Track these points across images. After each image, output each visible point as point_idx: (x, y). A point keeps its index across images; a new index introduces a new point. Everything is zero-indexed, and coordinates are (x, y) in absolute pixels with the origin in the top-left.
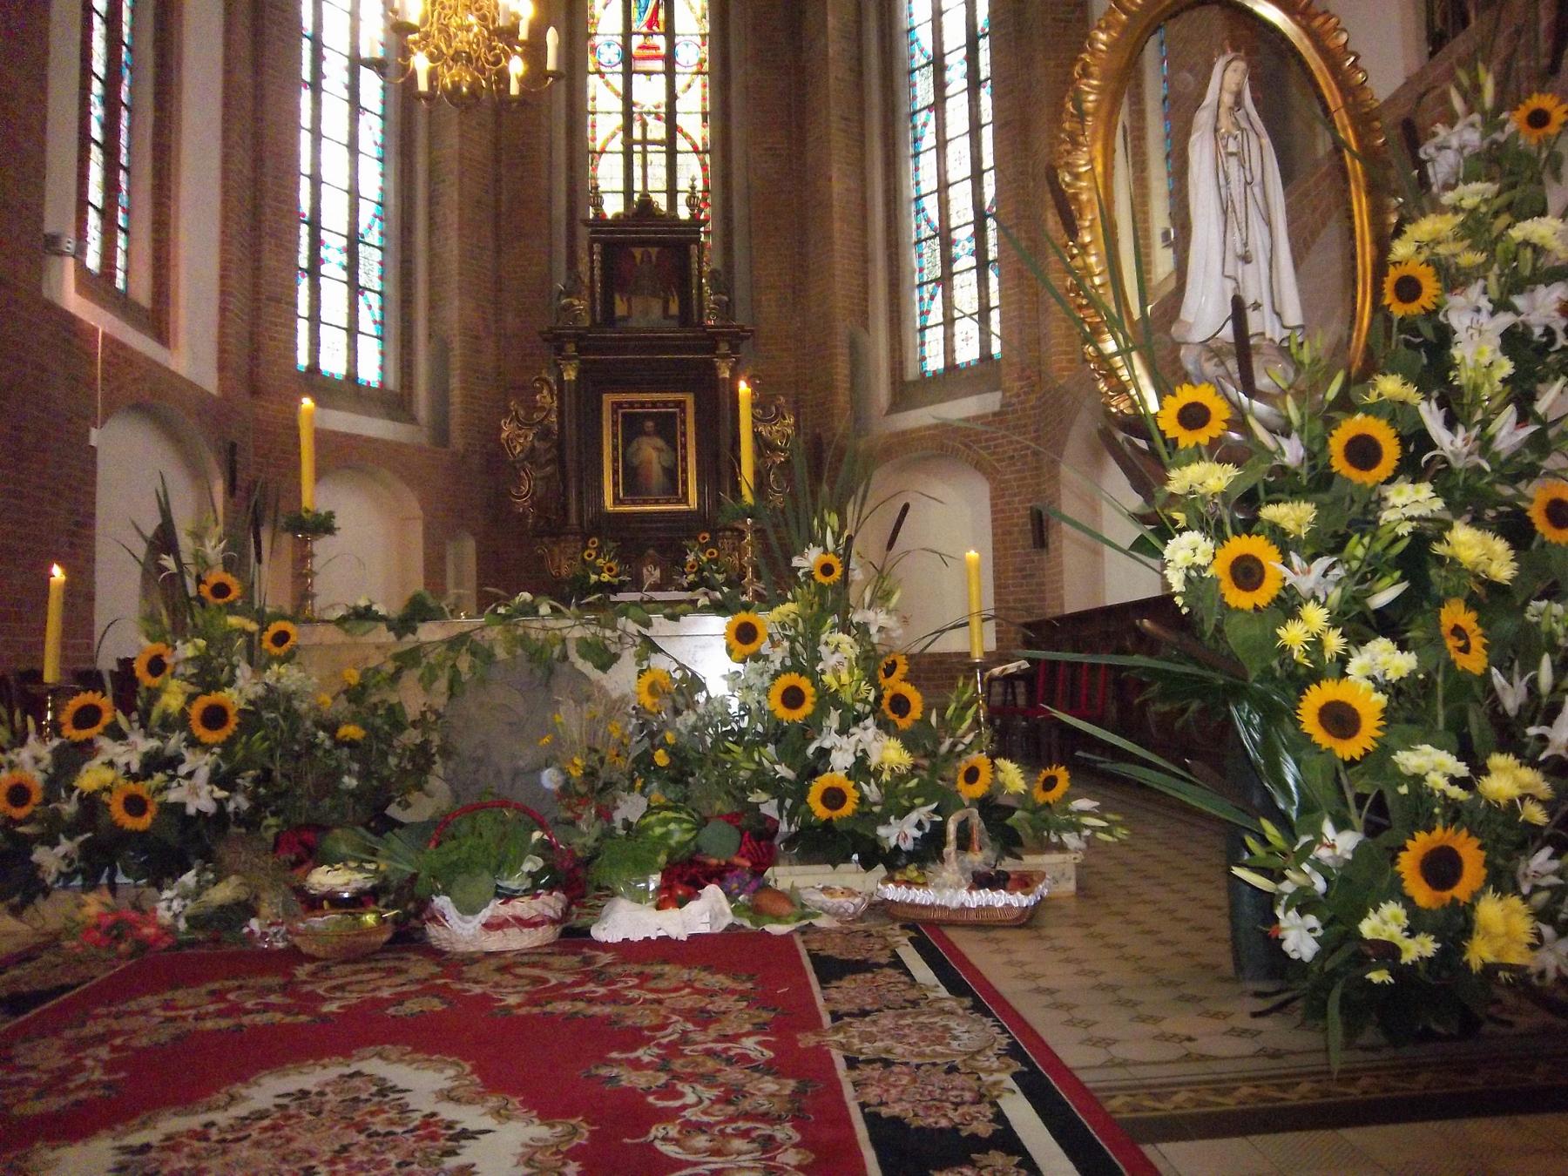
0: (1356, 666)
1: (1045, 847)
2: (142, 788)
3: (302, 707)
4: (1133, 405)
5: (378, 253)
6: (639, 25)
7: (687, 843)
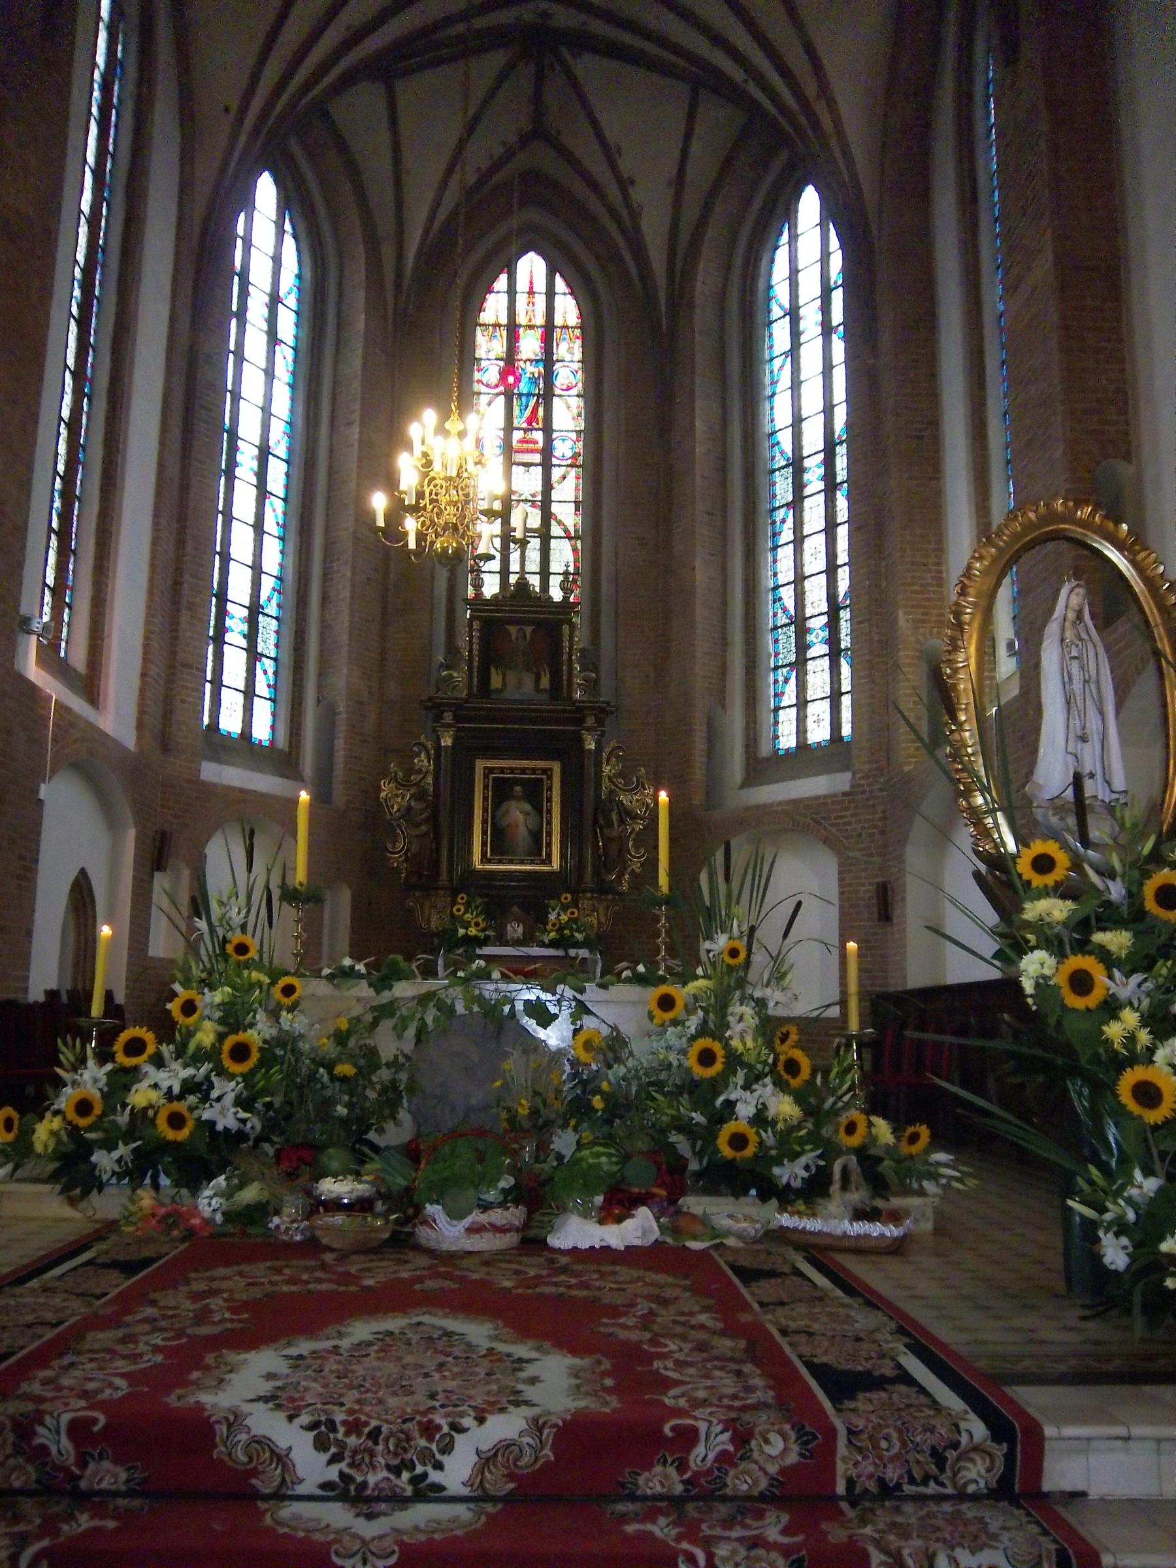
0: (1161, 1055)
1: (907, 1192)
2: (181, 1107)
3: (304, 1046)
4: (996, 847)
5: (275, 622)
6: (519, 421)
7: (615, 1174)
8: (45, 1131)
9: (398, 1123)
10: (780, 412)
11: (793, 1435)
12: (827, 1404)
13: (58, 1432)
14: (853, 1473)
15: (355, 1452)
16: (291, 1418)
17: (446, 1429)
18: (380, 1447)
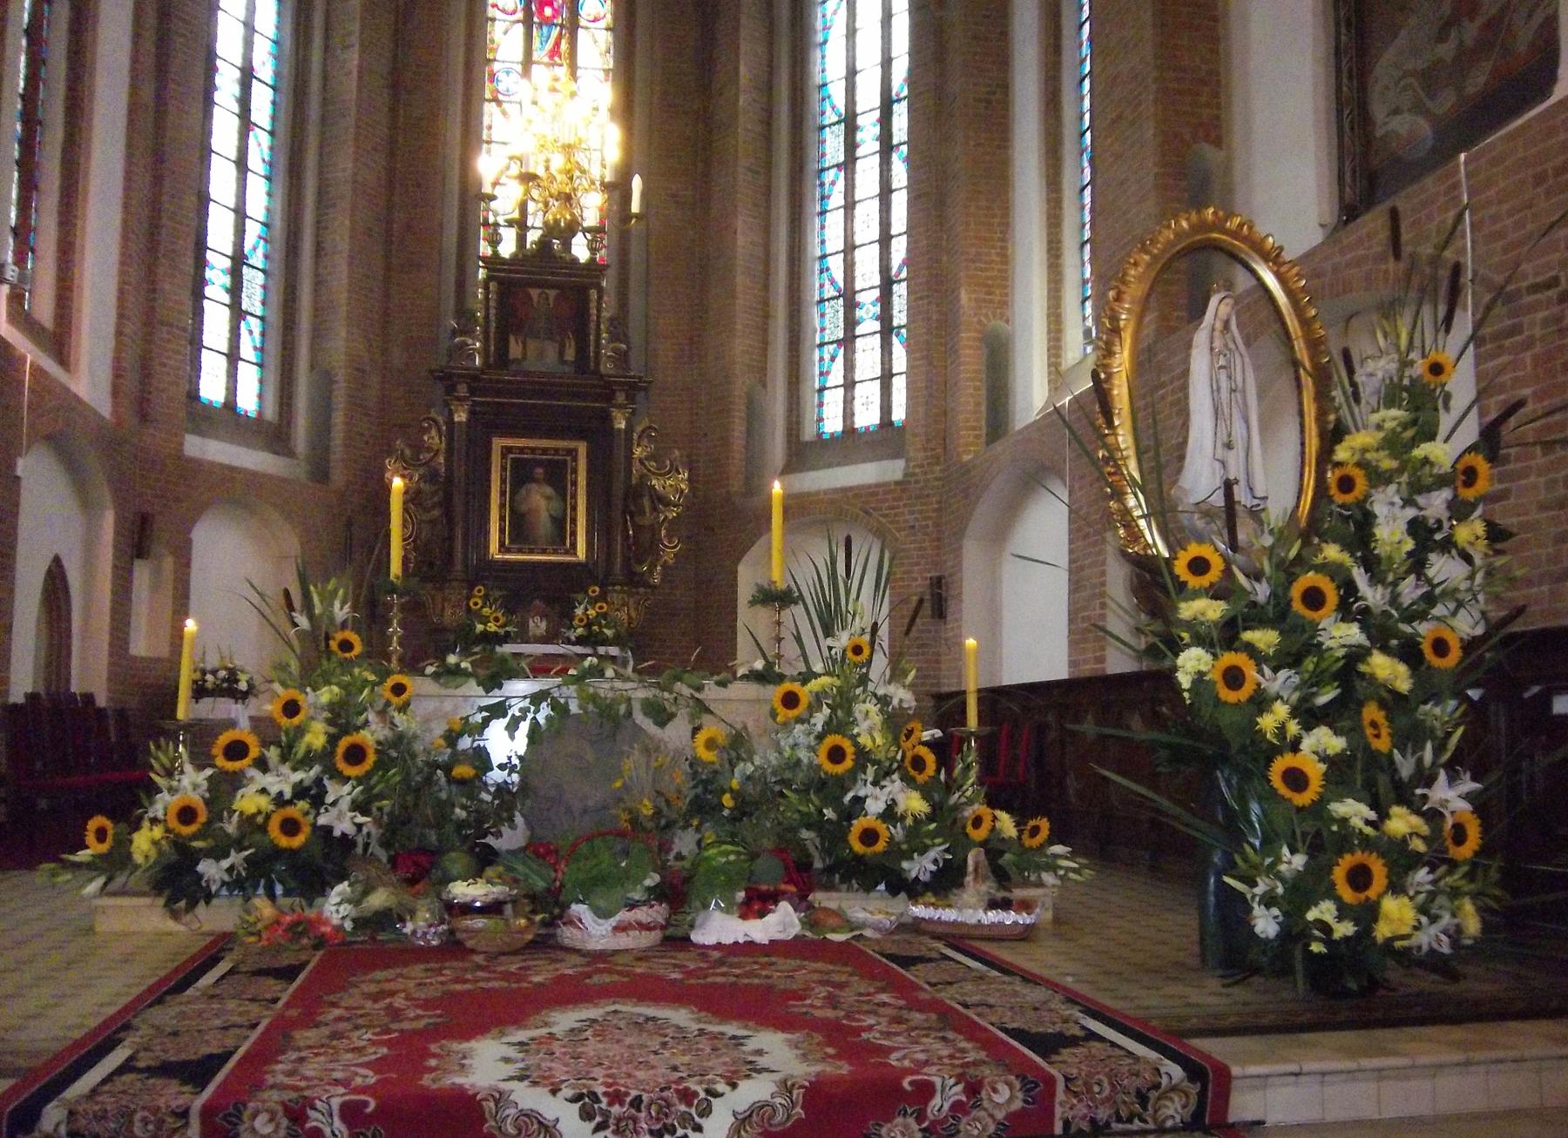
0: (1308, 743)
1: (1026, 883)
3: (418, 747)
5: (261, 275)
8: (144, 842)
9: (513, 827)
10: (830, 65)
11: (1018, 1085)
12: (1038, 1059)
13: (331, 1115)
14: (1070, 1115)
15: (619, 1120)
16: (554, 1092)
17: (702, 1095)
18: (643, 1115)
